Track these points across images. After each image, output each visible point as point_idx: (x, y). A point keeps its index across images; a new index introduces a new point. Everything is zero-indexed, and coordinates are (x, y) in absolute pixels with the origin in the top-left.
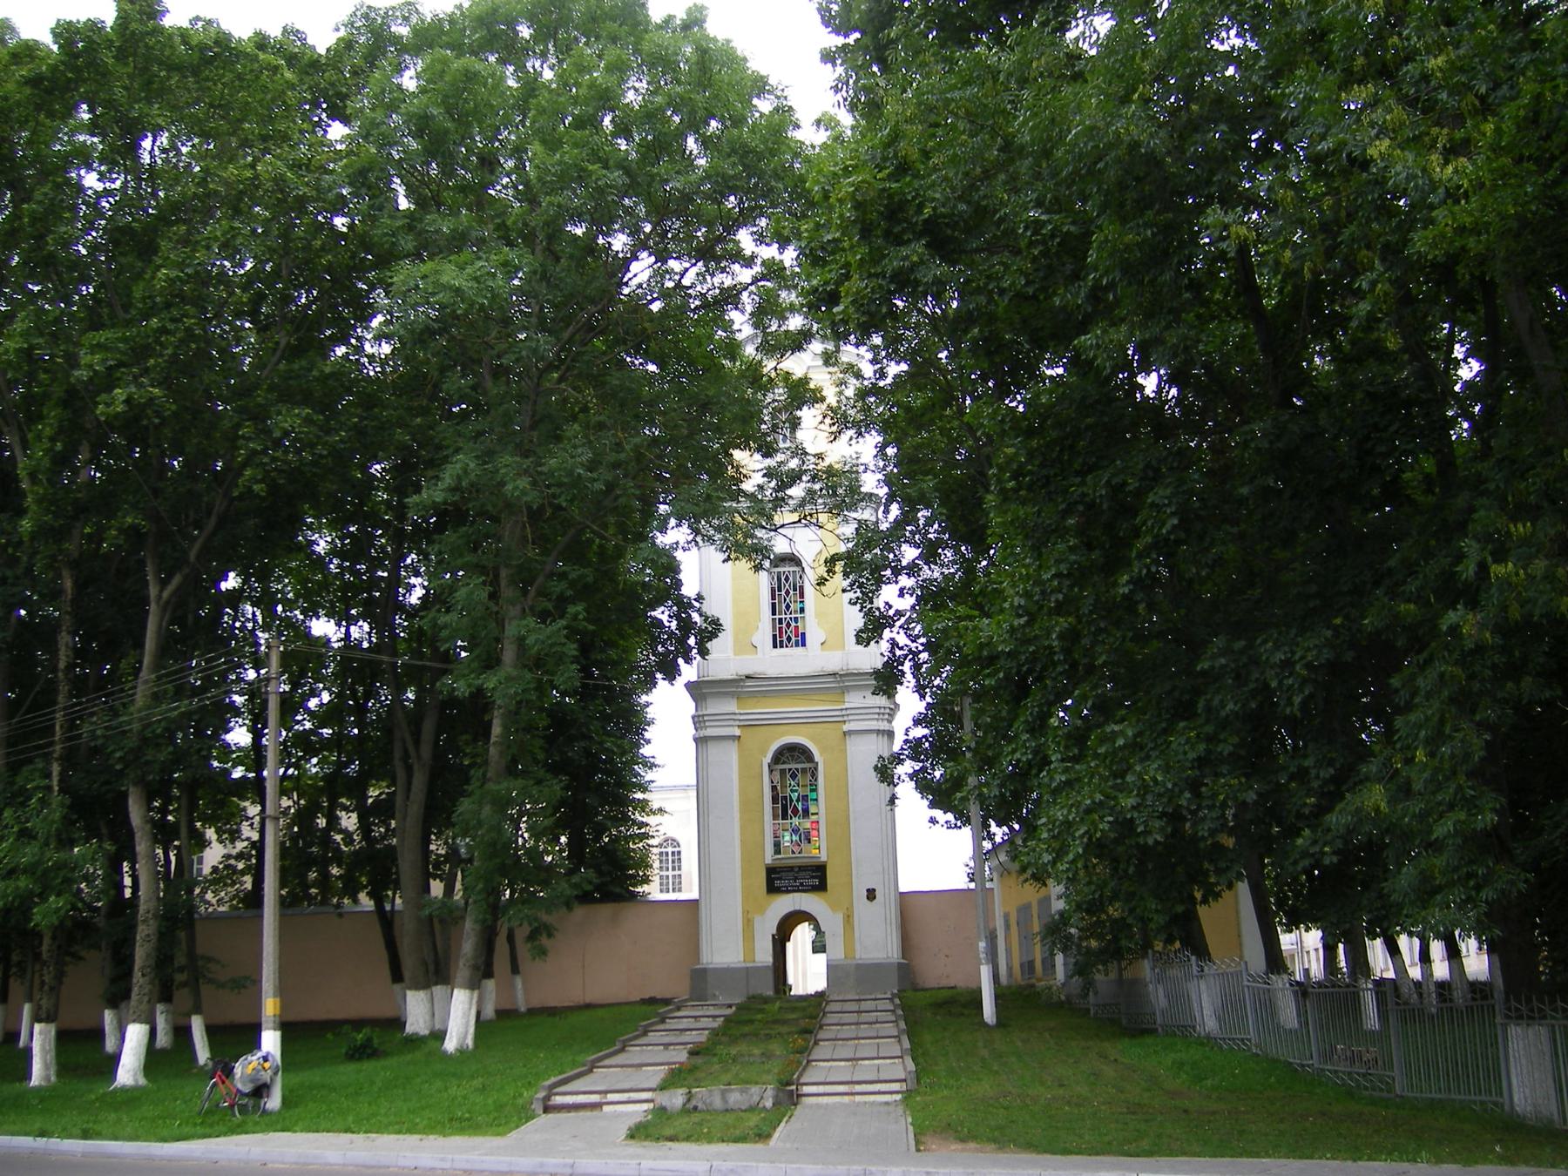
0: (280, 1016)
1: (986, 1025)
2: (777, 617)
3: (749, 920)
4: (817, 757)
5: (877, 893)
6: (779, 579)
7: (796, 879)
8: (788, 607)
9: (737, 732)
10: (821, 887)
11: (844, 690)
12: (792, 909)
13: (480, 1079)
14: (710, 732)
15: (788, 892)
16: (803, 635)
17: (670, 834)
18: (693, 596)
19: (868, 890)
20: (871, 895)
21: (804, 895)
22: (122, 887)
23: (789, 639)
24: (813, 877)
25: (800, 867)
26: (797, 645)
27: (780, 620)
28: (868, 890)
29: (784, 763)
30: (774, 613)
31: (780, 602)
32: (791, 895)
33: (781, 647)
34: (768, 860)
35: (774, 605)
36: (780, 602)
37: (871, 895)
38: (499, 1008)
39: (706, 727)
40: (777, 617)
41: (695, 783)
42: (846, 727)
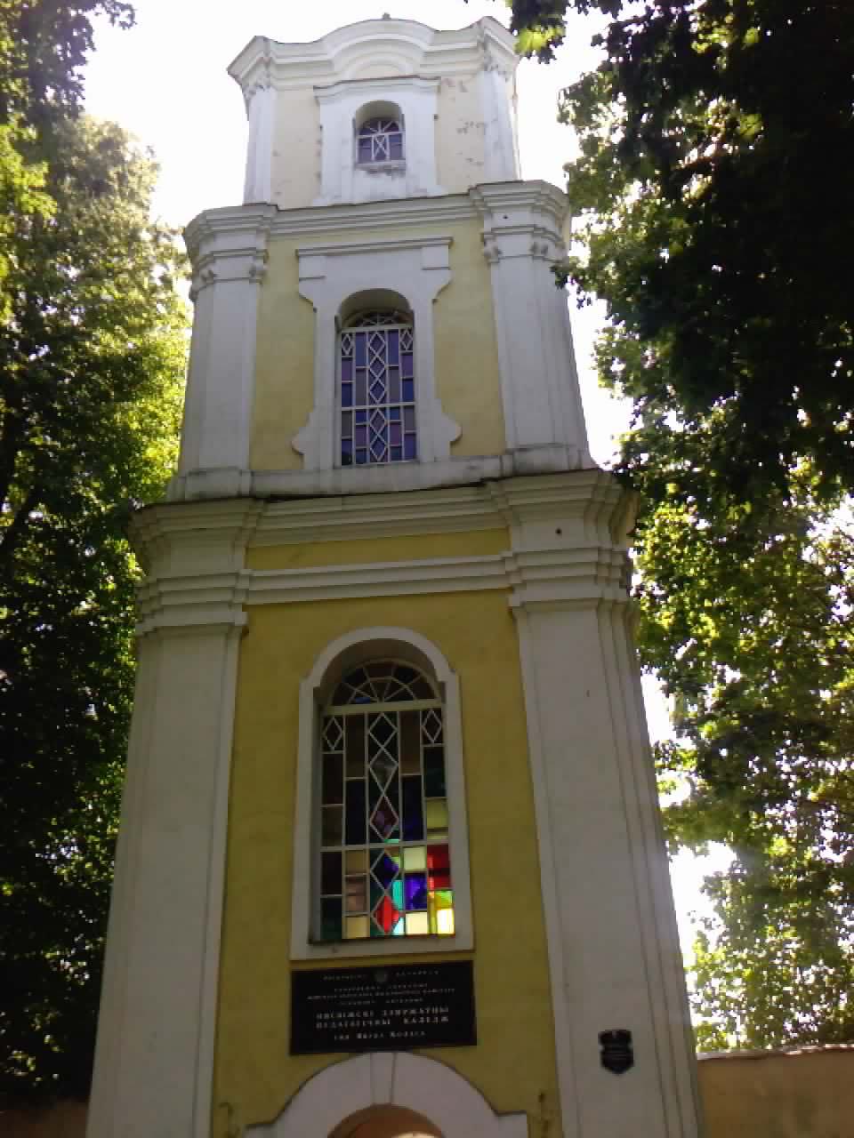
2: (354, 408)
4: (442, 672)
5: (639, 1046)
7: (378, 1007)
8: (377, 388)
11: (509, 520)
15: (357, 1048)
17: (305, 945)
19: (605, 1038)
21: (405, 1059)
22: (418, 983)
23: (378, 445)
24: (430, 1001)
25: (392, 970)
26: (397, 456)
27: (361, 414)
28: (605, 1038)
29: (359, 700)
30: (347, 401)
32: (363, 1060)
33: (361, 461)
34: (300, 949)
39: (162, 609)
40: (354, 408)
41: (409, 932)
42: (514, 600)
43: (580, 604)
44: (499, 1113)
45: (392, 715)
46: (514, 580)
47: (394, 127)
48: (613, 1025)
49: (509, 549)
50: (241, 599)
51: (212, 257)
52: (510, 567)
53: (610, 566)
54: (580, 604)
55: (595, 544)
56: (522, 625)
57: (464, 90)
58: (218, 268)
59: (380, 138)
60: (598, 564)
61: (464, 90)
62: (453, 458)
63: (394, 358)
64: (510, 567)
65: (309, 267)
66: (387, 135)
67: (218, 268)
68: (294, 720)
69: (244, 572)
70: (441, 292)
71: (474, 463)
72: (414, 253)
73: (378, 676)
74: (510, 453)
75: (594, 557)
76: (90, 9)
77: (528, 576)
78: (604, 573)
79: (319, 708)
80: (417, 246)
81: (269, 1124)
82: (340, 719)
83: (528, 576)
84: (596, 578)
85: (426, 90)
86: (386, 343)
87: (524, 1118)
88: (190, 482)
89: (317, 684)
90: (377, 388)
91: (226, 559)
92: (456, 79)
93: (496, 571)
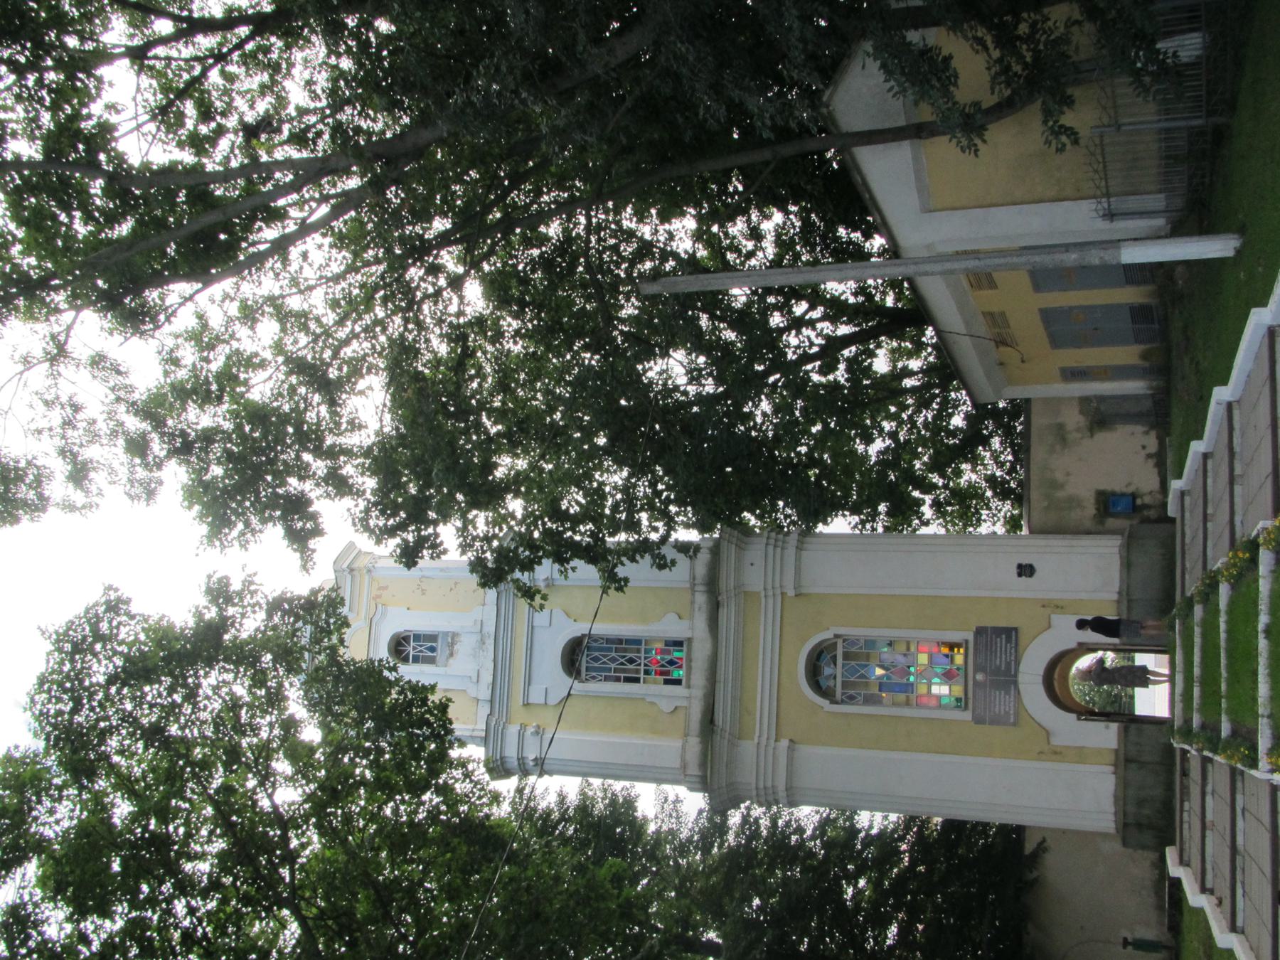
0: (1122, 752)
1: (1239, 252)
2: (642, 676)
3: (1055, 753)
4: (828, 635)
5: (1025, 561)
6: (596, 669)
8: (631, 661)
9: (784, 743)
10: (1010, 634)
12: (1040, 679)
13: (328, 416)
14: (781, 786)
16: (668, 643)
18: (382, 652)
19: (1020, 575)
20: (1026, 570)
28: (1020, 575)
30: (637, 680)
31: (624, 671)
35: (628, 680)
36: (624, 671)
37: (1026, 570)
38: (1028, 833)
40: (642, 676)
42: (791, 593)
43: (798, 559)
44: (1049, 627)
45: (844, 665)
46: (778, 592)
47: (406, 639)
48: (1015, 571)
49: (758, 593)
50: (772, 741)
51: (522, 760)
52: (770, 593)
53: (776, 540)
54: (798, 559)
55: (763, 546)
56: (804, 591)
57: (385, 588)
58: (531, 755)
59: (414, 648)
60: (775, 546)
61: (385, 588)
62: (691, 618)
63: (610, 650)
64: (770, 593)
65: (536, 696)
66: (412, 643)
67: (531, 755)
68: (846, 715)
69: (756, 741)
70: (568, 615)
71: (697, 606)
72: (536, 630)
73: (1174, 590)
74: (693, 585)
75: (771, 548)
76: (1273, 572)
77: (777, 585)
78: (780, 543)
79: (837, 703)
80: (532, 629)
81: (1048, 733)
82: (843, 694)
83: (777, 585)
84: (783, 549)
85: (384, 614)
86: (597, 654)
87: (1053, 616)
88: (689, 772)
89: (827, 702)
90: (631, 661)
91: (748, 748)
92: (375, 592)
93: (771, 601)
